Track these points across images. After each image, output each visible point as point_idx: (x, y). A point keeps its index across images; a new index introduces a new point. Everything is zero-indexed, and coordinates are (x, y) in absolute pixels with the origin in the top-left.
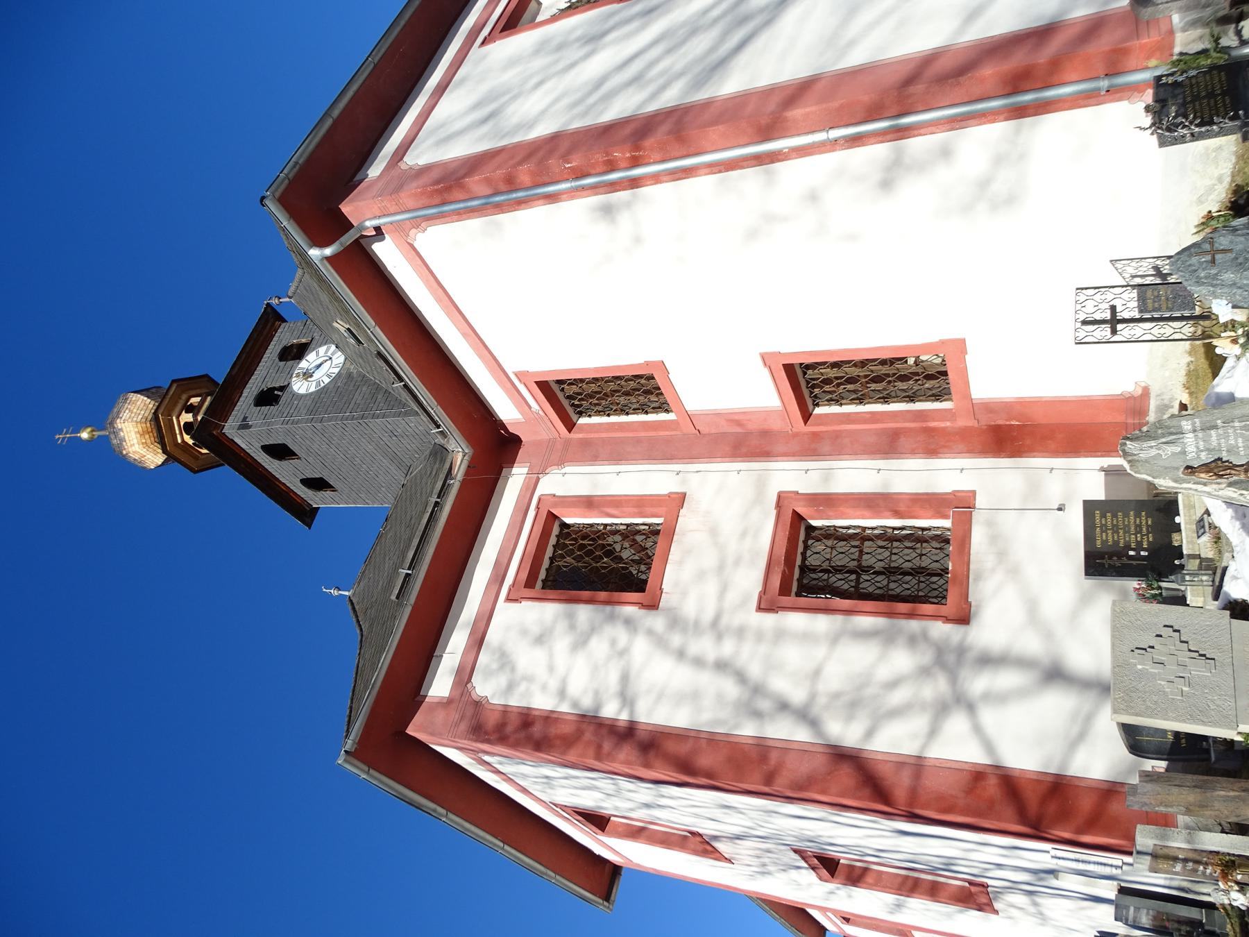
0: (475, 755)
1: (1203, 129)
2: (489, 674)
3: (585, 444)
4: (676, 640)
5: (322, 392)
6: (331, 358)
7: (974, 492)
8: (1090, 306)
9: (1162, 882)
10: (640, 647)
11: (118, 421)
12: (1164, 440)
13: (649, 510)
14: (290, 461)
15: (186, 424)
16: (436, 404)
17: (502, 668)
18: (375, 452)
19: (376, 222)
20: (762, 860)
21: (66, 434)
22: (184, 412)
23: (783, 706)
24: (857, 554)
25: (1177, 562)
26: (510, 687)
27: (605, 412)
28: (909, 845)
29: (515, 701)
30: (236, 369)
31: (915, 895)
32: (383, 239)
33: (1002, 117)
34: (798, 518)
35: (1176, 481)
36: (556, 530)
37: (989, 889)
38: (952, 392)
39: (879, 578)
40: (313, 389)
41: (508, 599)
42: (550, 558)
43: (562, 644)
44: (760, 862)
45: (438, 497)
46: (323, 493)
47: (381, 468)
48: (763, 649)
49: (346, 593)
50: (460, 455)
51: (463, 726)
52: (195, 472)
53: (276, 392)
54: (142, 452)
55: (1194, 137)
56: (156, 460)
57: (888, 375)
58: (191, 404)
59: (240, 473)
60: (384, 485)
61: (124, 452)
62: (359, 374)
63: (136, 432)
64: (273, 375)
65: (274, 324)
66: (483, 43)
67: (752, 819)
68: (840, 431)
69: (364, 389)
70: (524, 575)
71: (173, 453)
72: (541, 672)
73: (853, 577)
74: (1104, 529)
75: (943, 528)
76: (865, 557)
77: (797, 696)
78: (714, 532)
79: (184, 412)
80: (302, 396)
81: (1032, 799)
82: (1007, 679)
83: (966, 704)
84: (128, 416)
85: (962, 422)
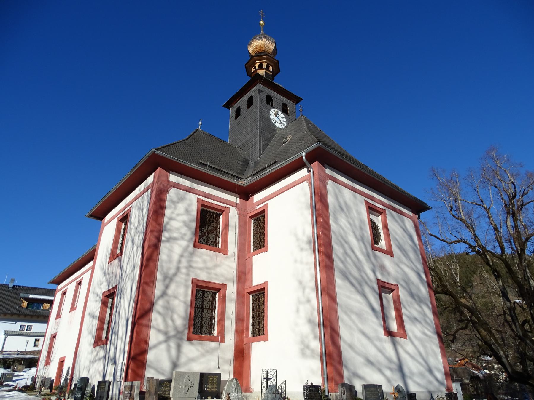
0: (151, 187)
1: (306, 395)
2: (177, 194)
3: (245, 223)
4: (186, 254)
5: (269, 120)
7: (224, 343)
8: (272, 373)
9: (114, 392)
10: (184, 243)
11: (265, 39)
12: (236, 389)
13: (223, 244)
14: (247, 105)
17: (179, 199)
19: (312, 171)
20: (111, 274)
23: (167, 287)
24: (207, 308)
25: (203, 397)
26: (173, 202)
27: (255, 229)
28: (123, 322)
29: (167, 204)
31: (99, 323)
32: (308, 172)
33: (321, 351)
34: (219, 290)
35: (226, 391)
36: (218, 212)
37: (105, 345)
38: (254, 337)
39: (200, 315)
40: (271, 117)
41: (198, 199)
42: (210, 211)
43: (185, 218)
44: (110, 273)
45: (231, 174)
46: (235, 114)
47: (242, 138)
48: (183, 281)
49: (200, 128)
50: (243, 183)
51: (162, 187)
53: (271, 102)
55: (304, 393)
56: (250, 50)
57: (260, 318)
58: (270, 67)
61: (254, 40)
63: (261, 45)
66: (365, 201)
67: (130, 274)
68: (244, 303)
70: (206, 204)
71: (253, 59)
72: (177, 212)
73: (201, 307)
74: (213, 378)
75: (214, 333)
76: (206, 310)
77: (170, 291)
78: (216, 266)
80: (269, 113)
81: (141, 358)
82: (174, 352)
83: (168, 339)
84: (267, 43)
85: (245, 340)
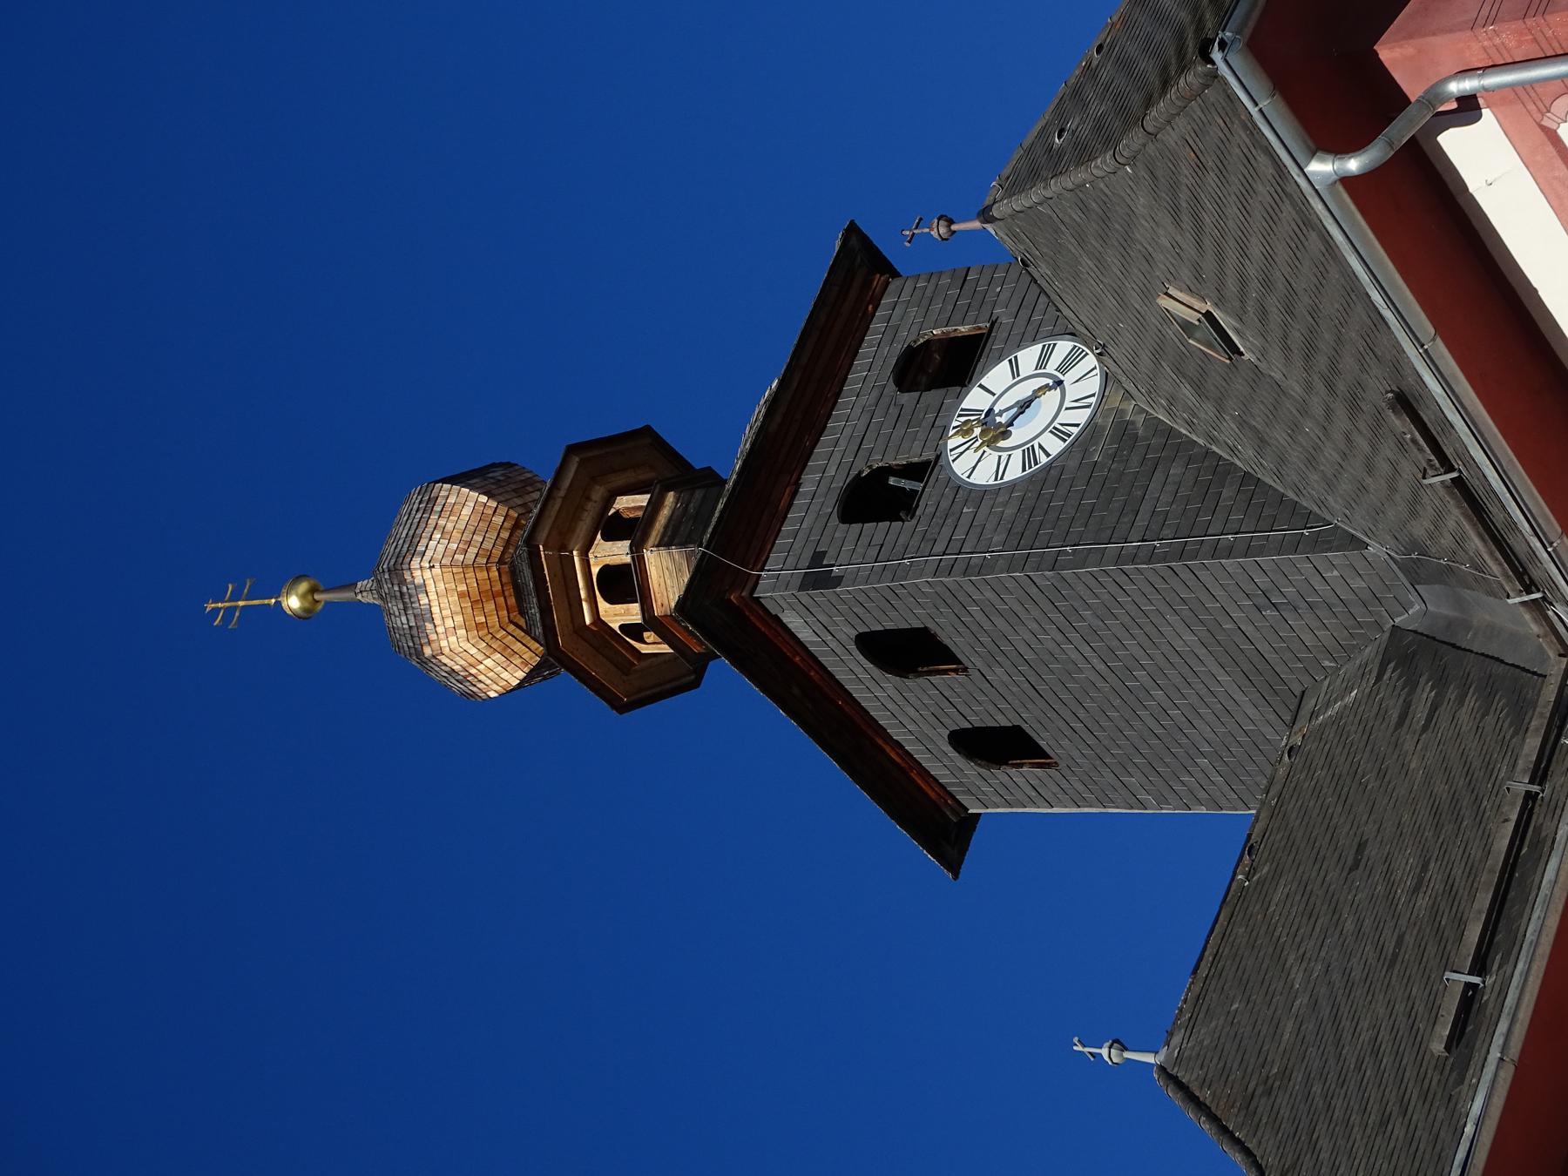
6: (1059, 383)
11: (415, 563)
14: (935, 679)
15: (606, 570)
16: (1560, 530)
18: (1202, 652)
21: (235, 598)
22: (599, 536)
30: (778, 418)
40: (1014, 472)
47: (1210, 700)
49: (1149, 1058)
52: (622, 708)
53: (892, 481)
54: (473, 651)
56: (505, 675)
58: (617, 512)
59: (791, 713)
60: (1206, 748)
61: (428, 651)
62: (1154, 425)
63: (461, 595)
64: (885, 431)
65: (867, 283)
69: (1175, 471)
80: (984, 492)
84: (441, 548)
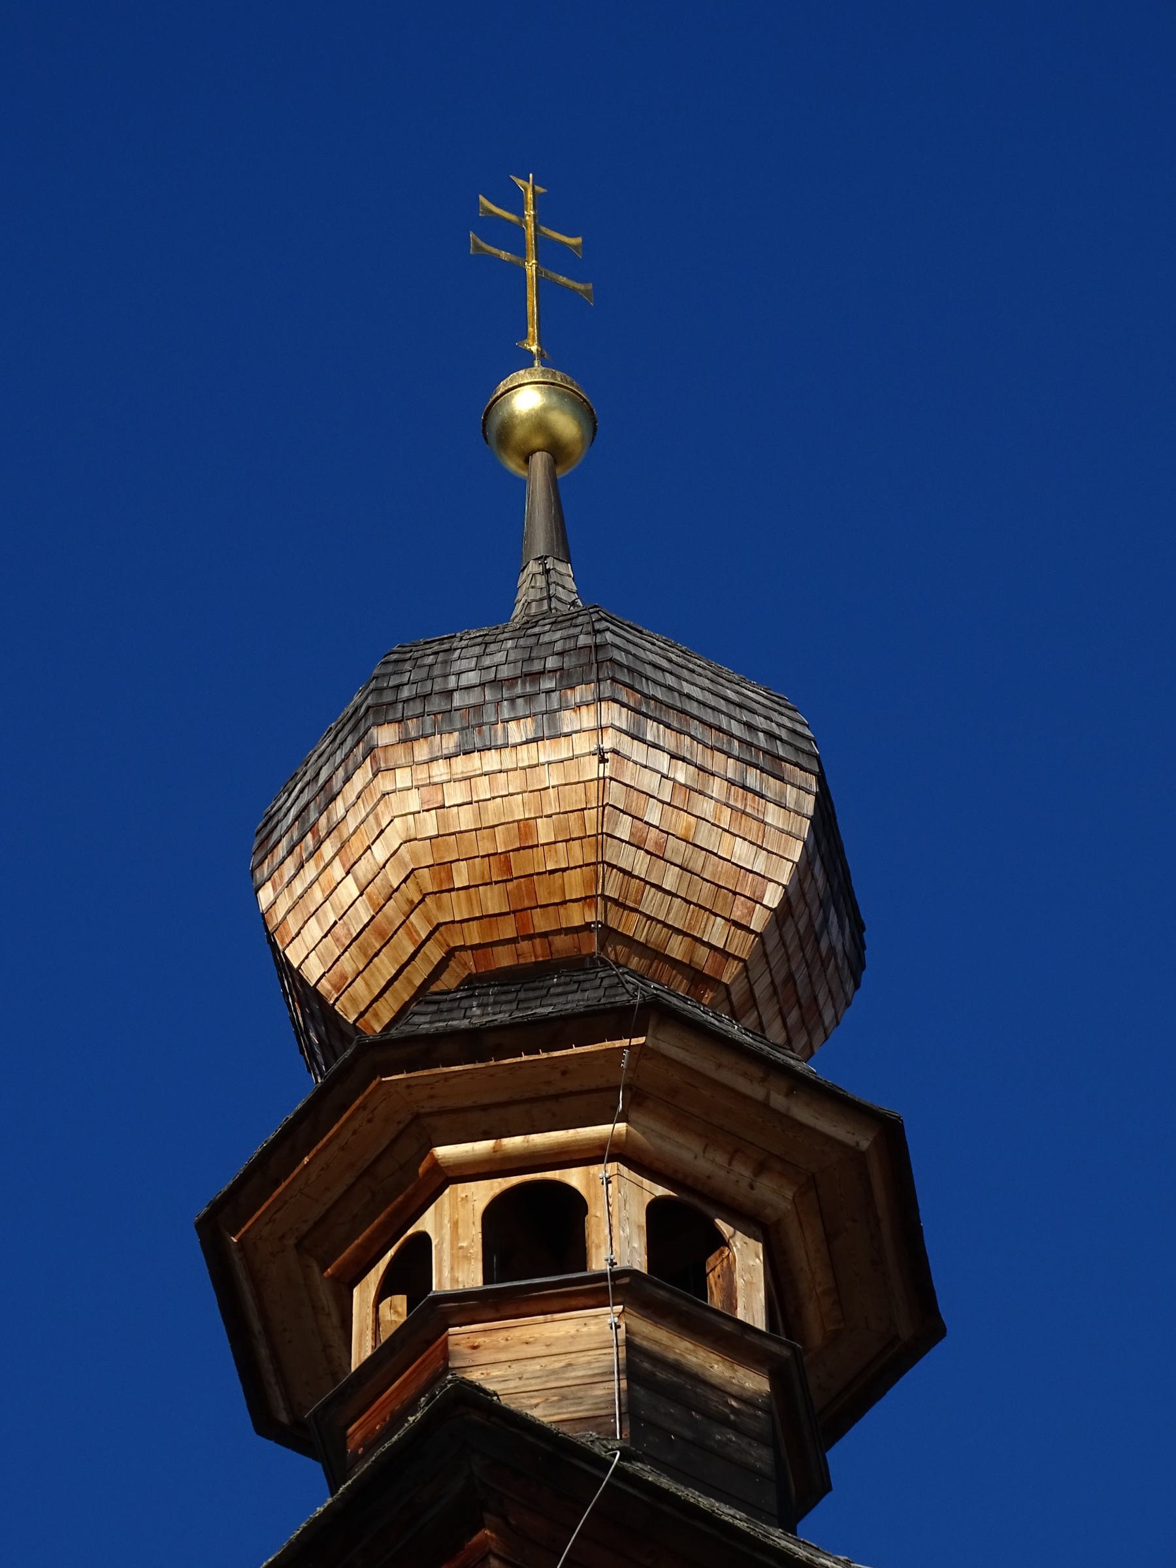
22: (661, 1191)
54: (380, 852)
56: (314, 931)
58: (721, 1242)
61: (385, 735)
63: (525, 827)
79: (661, 1191)
84: (649, 782)
